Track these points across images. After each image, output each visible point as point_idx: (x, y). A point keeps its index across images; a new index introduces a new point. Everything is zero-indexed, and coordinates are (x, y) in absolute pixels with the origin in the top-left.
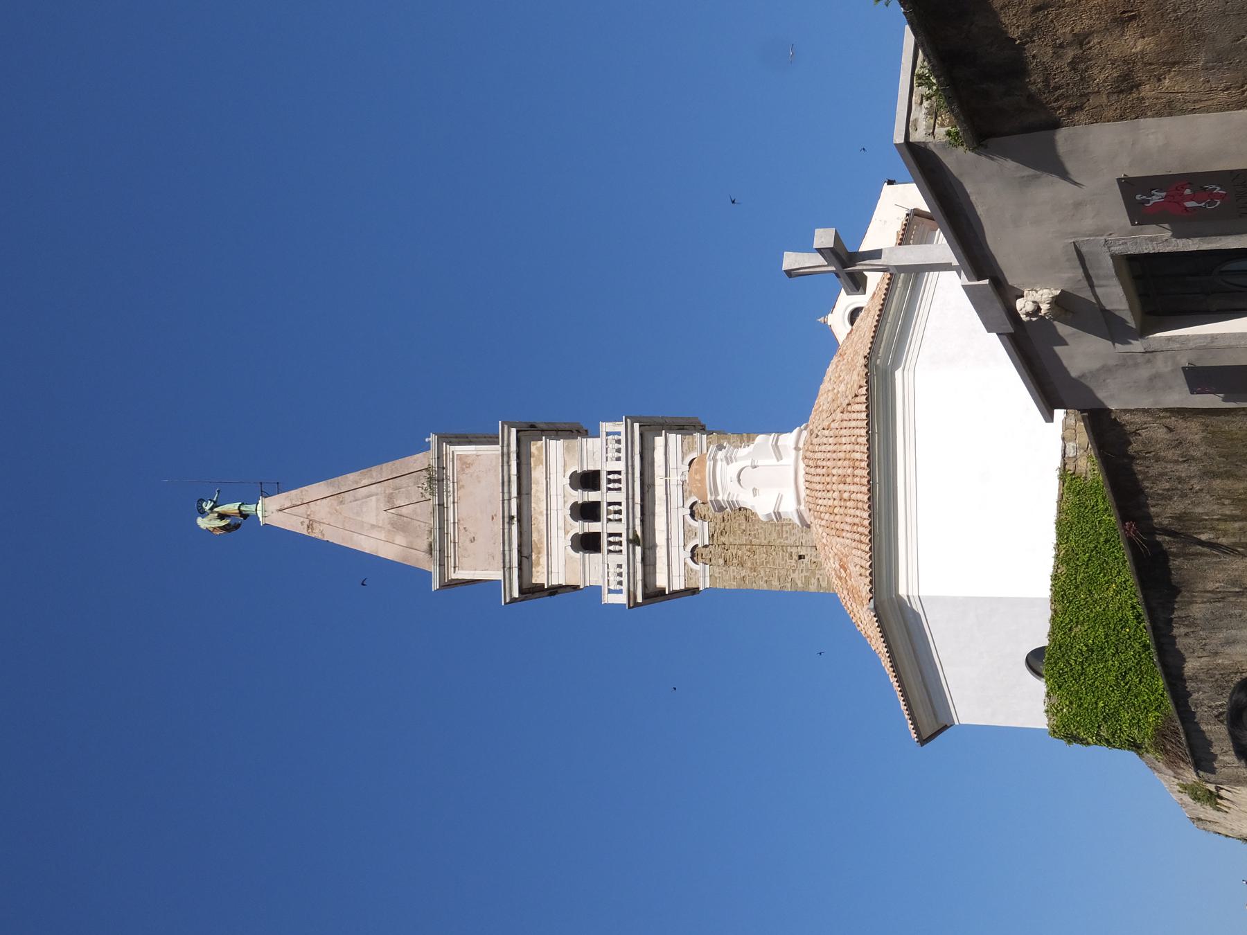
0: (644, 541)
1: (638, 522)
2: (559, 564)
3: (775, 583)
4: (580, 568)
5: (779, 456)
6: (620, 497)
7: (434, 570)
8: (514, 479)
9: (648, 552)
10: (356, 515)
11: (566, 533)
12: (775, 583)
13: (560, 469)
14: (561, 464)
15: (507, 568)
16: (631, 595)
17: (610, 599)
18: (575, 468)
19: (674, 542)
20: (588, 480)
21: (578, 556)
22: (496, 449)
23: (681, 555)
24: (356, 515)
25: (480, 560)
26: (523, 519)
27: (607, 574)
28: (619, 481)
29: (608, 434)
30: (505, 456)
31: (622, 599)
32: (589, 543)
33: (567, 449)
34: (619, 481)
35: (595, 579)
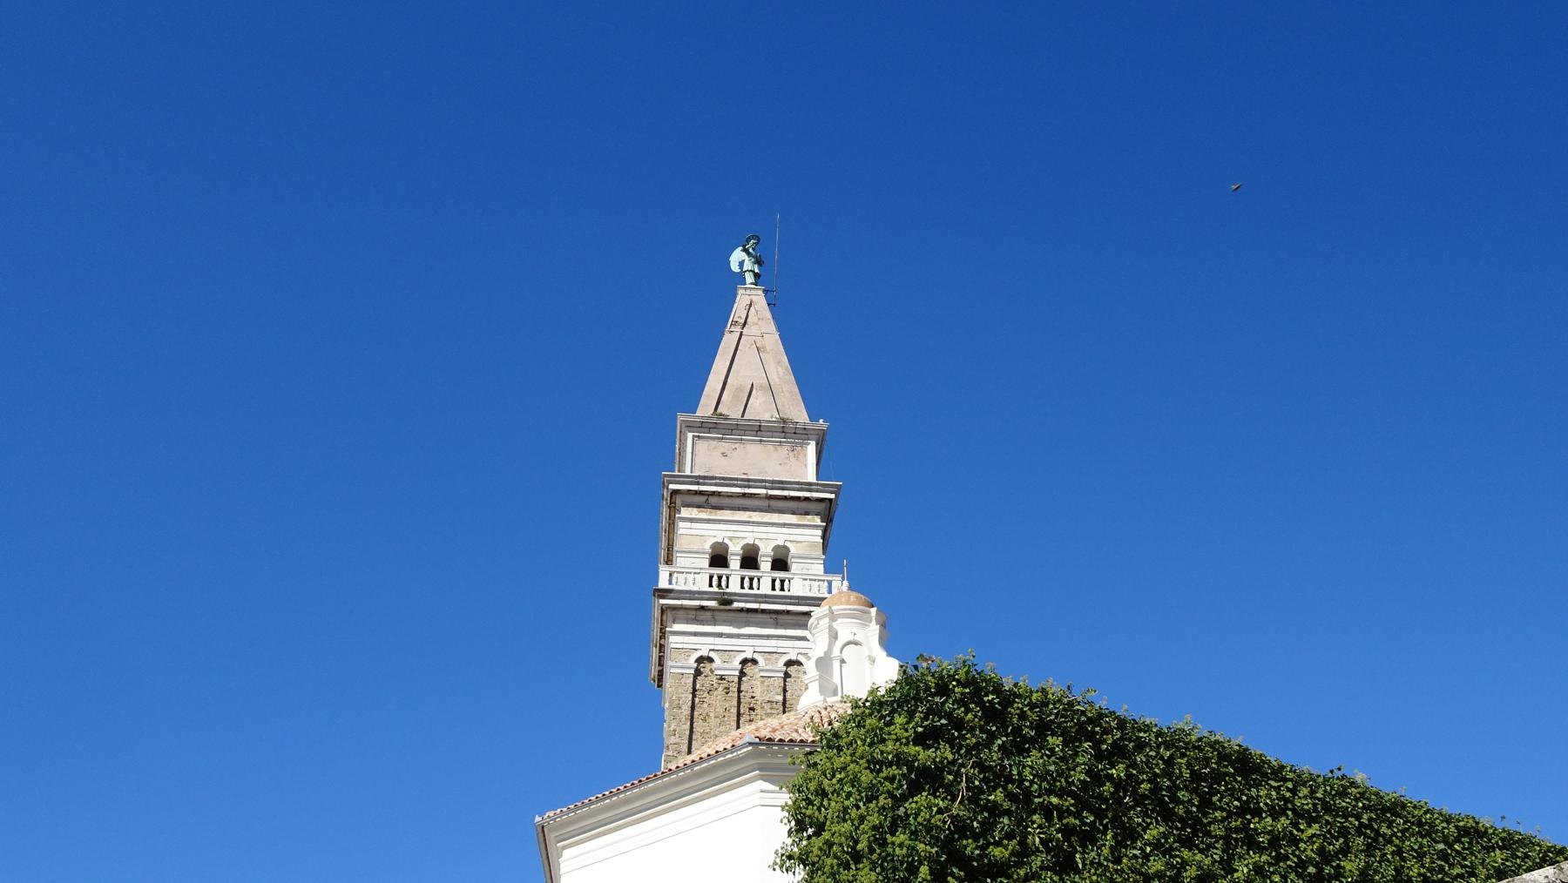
0: (724, 608)
1: (742, 605)
2: (698, 532)
3: (672, 740)
4: (696, 548)
5: (919, 740)
6: (765, 588)
7: (689, 418)
8: (786, 493)
9: (709, 614)
10: (753, 362)
11: (731, 539)
12: (672, 740)
13: (792, 538)
14: (799, 538)
15: (698, 480)
16: (664, 593)
17: (664, 573)
18: (793, 550)
19: (718, 640)
20: (780, 564)
21: (707, 547)
22: (811, 477)
23: (704, 646)
24: (753, 362)
25: (704, 458)
26: (745, 502)
27: (688, 573)
28: (751, 588)
29: (830, 583)
30: (808, 486)
31: (663, 583)
32: (719, 559)
33: (813, 544)
34: (751, 588)
35: (681, 561)
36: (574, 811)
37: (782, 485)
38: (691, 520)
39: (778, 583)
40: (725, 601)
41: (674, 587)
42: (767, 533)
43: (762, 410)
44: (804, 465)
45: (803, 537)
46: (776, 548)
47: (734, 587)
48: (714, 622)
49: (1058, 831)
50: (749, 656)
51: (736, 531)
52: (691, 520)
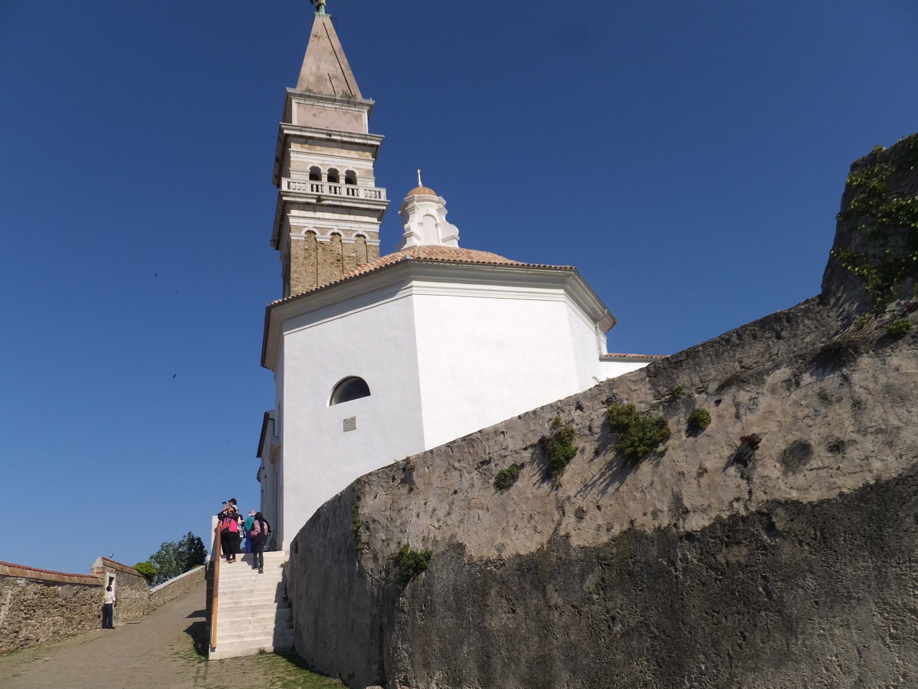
0: (318, 205)
1: (330, 202)
8: (352, 140)
9: (311, 207)
10: (323, 57)
11: (321, 165)
18: (358, 173)
19: (318, 222)
20: (351, 179)
22: (365, 130)
23: (310, 225)
24: (323, 57)
32: (315, 175)
33: (368, 171)
35: (294, 176)
36: (555, 269)
37: (350, 135)
38: (298, 152)
39: (315, 189)
40: (319, 199)
41: (291, 190)
42: (344, 161)
43: (327, 90)
44: (358, 123)
45: (363, 165)
46: (348, 172)
47: (326, 192)
48: (315, 211)
49: (882, 217)
50: (360, 233)
51: (326, 160)
52: (298, 152)
